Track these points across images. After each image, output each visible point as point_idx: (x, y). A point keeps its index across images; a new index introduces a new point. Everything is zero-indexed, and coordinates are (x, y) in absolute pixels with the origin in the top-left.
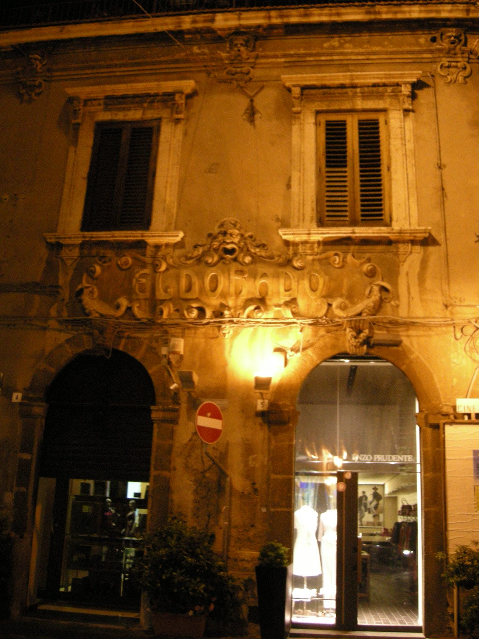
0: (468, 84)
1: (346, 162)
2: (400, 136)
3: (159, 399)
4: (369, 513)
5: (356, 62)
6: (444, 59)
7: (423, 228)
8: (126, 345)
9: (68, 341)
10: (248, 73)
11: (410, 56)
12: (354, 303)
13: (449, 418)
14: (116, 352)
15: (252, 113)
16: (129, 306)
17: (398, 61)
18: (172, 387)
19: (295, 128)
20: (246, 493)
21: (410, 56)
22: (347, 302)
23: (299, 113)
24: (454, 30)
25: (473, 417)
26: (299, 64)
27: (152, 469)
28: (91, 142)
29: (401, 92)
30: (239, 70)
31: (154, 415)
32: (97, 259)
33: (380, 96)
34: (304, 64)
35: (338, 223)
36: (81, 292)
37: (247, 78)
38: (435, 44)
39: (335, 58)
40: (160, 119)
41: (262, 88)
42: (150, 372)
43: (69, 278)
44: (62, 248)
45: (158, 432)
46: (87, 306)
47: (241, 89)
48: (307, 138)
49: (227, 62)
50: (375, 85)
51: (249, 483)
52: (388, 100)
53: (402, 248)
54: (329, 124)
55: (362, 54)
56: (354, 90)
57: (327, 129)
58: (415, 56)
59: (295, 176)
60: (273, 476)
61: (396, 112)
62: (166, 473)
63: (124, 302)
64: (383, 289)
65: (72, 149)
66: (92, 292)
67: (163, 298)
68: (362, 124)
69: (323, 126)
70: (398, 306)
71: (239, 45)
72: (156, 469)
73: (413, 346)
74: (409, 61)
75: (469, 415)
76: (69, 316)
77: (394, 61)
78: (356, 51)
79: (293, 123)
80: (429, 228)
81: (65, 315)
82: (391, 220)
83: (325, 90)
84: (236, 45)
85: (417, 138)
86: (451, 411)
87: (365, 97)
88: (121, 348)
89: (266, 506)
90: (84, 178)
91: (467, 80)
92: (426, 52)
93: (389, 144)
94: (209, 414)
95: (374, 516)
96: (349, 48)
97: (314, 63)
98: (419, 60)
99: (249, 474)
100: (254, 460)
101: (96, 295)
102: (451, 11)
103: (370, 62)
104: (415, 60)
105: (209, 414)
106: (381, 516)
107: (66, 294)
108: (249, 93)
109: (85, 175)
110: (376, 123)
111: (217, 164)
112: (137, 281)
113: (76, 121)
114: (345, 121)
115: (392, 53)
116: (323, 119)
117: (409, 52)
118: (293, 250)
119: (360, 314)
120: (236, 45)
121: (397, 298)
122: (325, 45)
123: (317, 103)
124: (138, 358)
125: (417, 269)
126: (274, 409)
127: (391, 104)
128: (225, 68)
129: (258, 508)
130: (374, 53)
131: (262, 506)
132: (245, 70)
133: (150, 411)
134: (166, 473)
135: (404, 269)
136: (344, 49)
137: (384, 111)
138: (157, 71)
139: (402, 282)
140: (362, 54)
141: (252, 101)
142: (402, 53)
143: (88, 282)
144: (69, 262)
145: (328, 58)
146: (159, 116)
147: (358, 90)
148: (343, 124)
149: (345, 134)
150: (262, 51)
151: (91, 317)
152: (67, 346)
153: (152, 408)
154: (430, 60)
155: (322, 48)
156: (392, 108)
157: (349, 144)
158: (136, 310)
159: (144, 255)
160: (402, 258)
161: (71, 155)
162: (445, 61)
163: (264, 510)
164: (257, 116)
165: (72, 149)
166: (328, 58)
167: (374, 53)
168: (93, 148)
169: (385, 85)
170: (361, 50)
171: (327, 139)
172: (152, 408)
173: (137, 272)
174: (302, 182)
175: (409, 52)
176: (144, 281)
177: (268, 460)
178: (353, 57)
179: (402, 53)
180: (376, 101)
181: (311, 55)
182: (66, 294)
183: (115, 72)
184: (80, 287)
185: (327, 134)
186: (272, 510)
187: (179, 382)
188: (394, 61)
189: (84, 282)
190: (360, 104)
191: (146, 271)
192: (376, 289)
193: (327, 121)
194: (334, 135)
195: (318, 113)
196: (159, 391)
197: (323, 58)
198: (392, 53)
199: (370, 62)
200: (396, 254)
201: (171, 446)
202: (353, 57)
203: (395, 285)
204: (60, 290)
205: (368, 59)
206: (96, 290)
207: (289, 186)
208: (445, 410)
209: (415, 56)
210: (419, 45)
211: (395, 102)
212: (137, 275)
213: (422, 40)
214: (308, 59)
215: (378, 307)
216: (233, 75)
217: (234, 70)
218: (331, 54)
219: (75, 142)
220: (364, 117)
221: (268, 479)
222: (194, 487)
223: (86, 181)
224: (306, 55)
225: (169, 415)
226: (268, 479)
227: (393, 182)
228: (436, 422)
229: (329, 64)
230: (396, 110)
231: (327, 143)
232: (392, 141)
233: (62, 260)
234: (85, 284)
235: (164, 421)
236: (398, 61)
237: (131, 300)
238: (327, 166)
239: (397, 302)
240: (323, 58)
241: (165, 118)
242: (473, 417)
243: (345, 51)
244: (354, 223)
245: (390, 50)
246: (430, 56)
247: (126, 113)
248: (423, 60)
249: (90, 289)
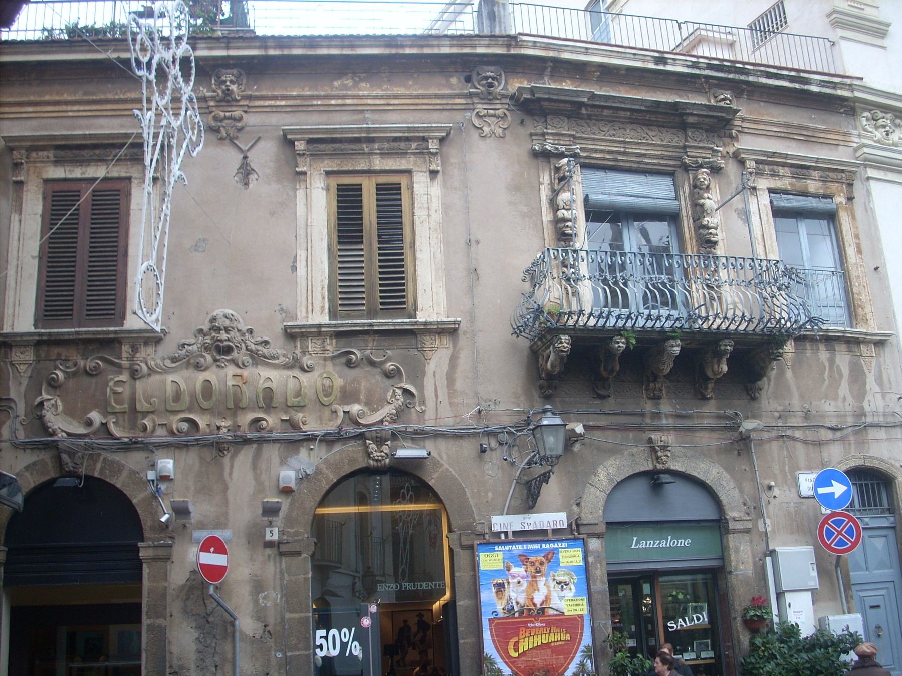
0: (507, 138)
1: (362, 237)
2: (428, 203)
3: (147, 534)
4: (414, 649)
5: (374, 108)
6: (479, 106)
7: (452, 320)
8: (102, 469)
9: (27, 468)
10: (240, 119)
11: (439, 101)
12: (374, 410)
13: (484, 539)
14: (88, 478)
15: (246, 171)
16: (104, 421)
17: (424, 107)
18: (163, 519)
19: (300, 194)
20: (257, 637)
21: (439, 101)
22: (366, 409)
23: (305, 173)
24: (492, 68)
25: (510, 535)
26: (304, 109)
27: (144, 617)
28: (39, 209)
29: (428, 148)
30: (227, 114)
31: (142, 554)
32: (58, 362)
33: (403, 154)
34: (310, 109)
35: (353, 313)
36: (41, 404)
37: (239, 125)
38: (469, 85)
39: (348, 101)
40: (129, 179)
41: (259, 139)
42: (135, 501)
43: (23, 388)
44: (11, 349)
45: (149, 574)
46: (49, 424)
47: (232, 140)
48: (316, 205)
49: (212, 103)
50: (396, 139)
51: (260, 625)
52: (412, 159)
53: (428, 342)
54: (341, 188)
55: (382, 97)
56: (371, 145)
57: (338, 196)
58: (444, 101)
59: (301, 255)
60: (288, 616)
61: (421, 174)
62: (160, 621)
63: (96, 416)
64: (406, 392)
65: (15, 218)
66: (55, 406)
67: (144, 409)
68: (381, 189)
69: (334, 191)
70: (424, 411)
71: (228, 83)
72: (149, 617)
73: (442, 458)
74: (438, 107)
75: (506, 533)
76: (25, 438)
77: (419, 107)
78: (374, 93)
79: (298, 187)
80: (459, 319)
81: (21, 436)
82: (416, 310)
83: (337, 145)
84: (225, 82)
85: (446, 208)
86: (487, 531)
87: (384, 154)
88: (96, 475)
89: (281, 651)
90: (33, 258)
91: (506, 131)
92: (458, 96)
93: (413, 214)
94: (212, 550)
95: (420, 653)
96: (365, 89)
97: (322, 108)
98: (449, 107)
99: (259, 615)
100: (264, 598)
101: (60, 408)
102: (488, 46)
103: (390, 108)
104: (445, 107)
105: (212, 550)
106: (430, 651)
107: (21, 408)
108: (242, 146)
109: (36, 253)
110: (397, 188)
111: (204, 240)
112: (112, 389)
113: (19, 179)
114: (361, 185)
115: (417, 97)
116: (334, 182)
117: (438, 96)
118: (301, 348)
119: (382, 421)
120: (225, 82)
121: (423, 402)
122: (336, 84)
123: (326, 162)
124: (118, 486)
125: (446, 367)
126: (285, 537)
127: (415, 163)
128: (211, 112)
129: (273, 653)
130: (396, 97)
131: (276, 651)
132: (237, 113)
133: (138, 550)
134: (160, 621)
135: (431, 367)
136: (360, 90)
137: (409, 172)
138: (124, 113)
139: (429, 382)
140: (382, 97)
141: (245, 158)
142: (429, 97)
143: (48, 393)
144: (22, 368)
145: (340, 102)
146: (128, 175)
147: (376, 146)
148: (358, 188)
149: (361, 201)
150: (257, 90)
151: (55, 438)
152: (27, 474)
153: (140, 544)
154: (463, 107)
155: (332, 87)
156: (417, 169)
157: (365, 216)
158: (112, 427)
159: (120, 358)
160: (429, 354)
161: (15, 225)
162: (480, 107)
163: (279, 655)
164: (253, 177)
165: (15, 218)
166: (340, 102)
167: (396, 97)
168: (43, 216)
169: (407, 139)
170: (380, 93)
171: (339, 207)
172: (140, 544)
173: (112, 379)
174: (309, 263)
175: (438, 96)
176: (119, 389)
177: (281, 598)
178: (369, 101)
179: (429, 97)
180: (398, 159)
181: (318, 97)
182: (21, 408)
183: (67, 111)
184: (39, 399)
185: (338, 202)
186: (289, 654)
187: (171, 511)
188: (419, 107)
189: (43, 393)
190: (378, 163)
191: (124, 377)
192: (399, 392)
193: (338, 185)
194: (348, 202)
195: (328, 173)
196: (147, 523)
197: (333, 102)
198: (417, 97)
199: (390, 108)
200: (422, 350)
201: (166, 588)
202: (369, 101)
203: (421, 387)
204: (12, 405)
205: (389, 104)
206: (59, 402)
207: (294, 268)
208: (479, 528)
209: (444, 101)
210: (451, 86)
211: (420, 161)
212: (111, 383)
213: (454, 80)
214: (315, 102)
215: (398, 416)
216: (221, 121)
217: (222, 114)
218: (344, 97)
219: (19, 208)
220: (383, 179)
221: (283, 619)
222: (197, 635)
223: (36, 262)
224: (312, 97)
225: (161, 552)
226: (283, 619)
227: (418, 263)
228: (470, 543)
229: (341, 109)
230: (421, 172)
231: (339, 213)
232: (417, 212)
233: (13, 365)
234: (45, 396)
235: (155, 559)
236: (424, 107)
237: (105, 413)
238: (339, 243)
239: (423, 407)
240: (333, 102)
241: (136, 178)
242: (510, 535)
243: (361, 93)
244: (372, 314)
245: (415, 93)
246: (462, 101)
247: (84, 169)
248: (454, 107)
249: (53, 402)
